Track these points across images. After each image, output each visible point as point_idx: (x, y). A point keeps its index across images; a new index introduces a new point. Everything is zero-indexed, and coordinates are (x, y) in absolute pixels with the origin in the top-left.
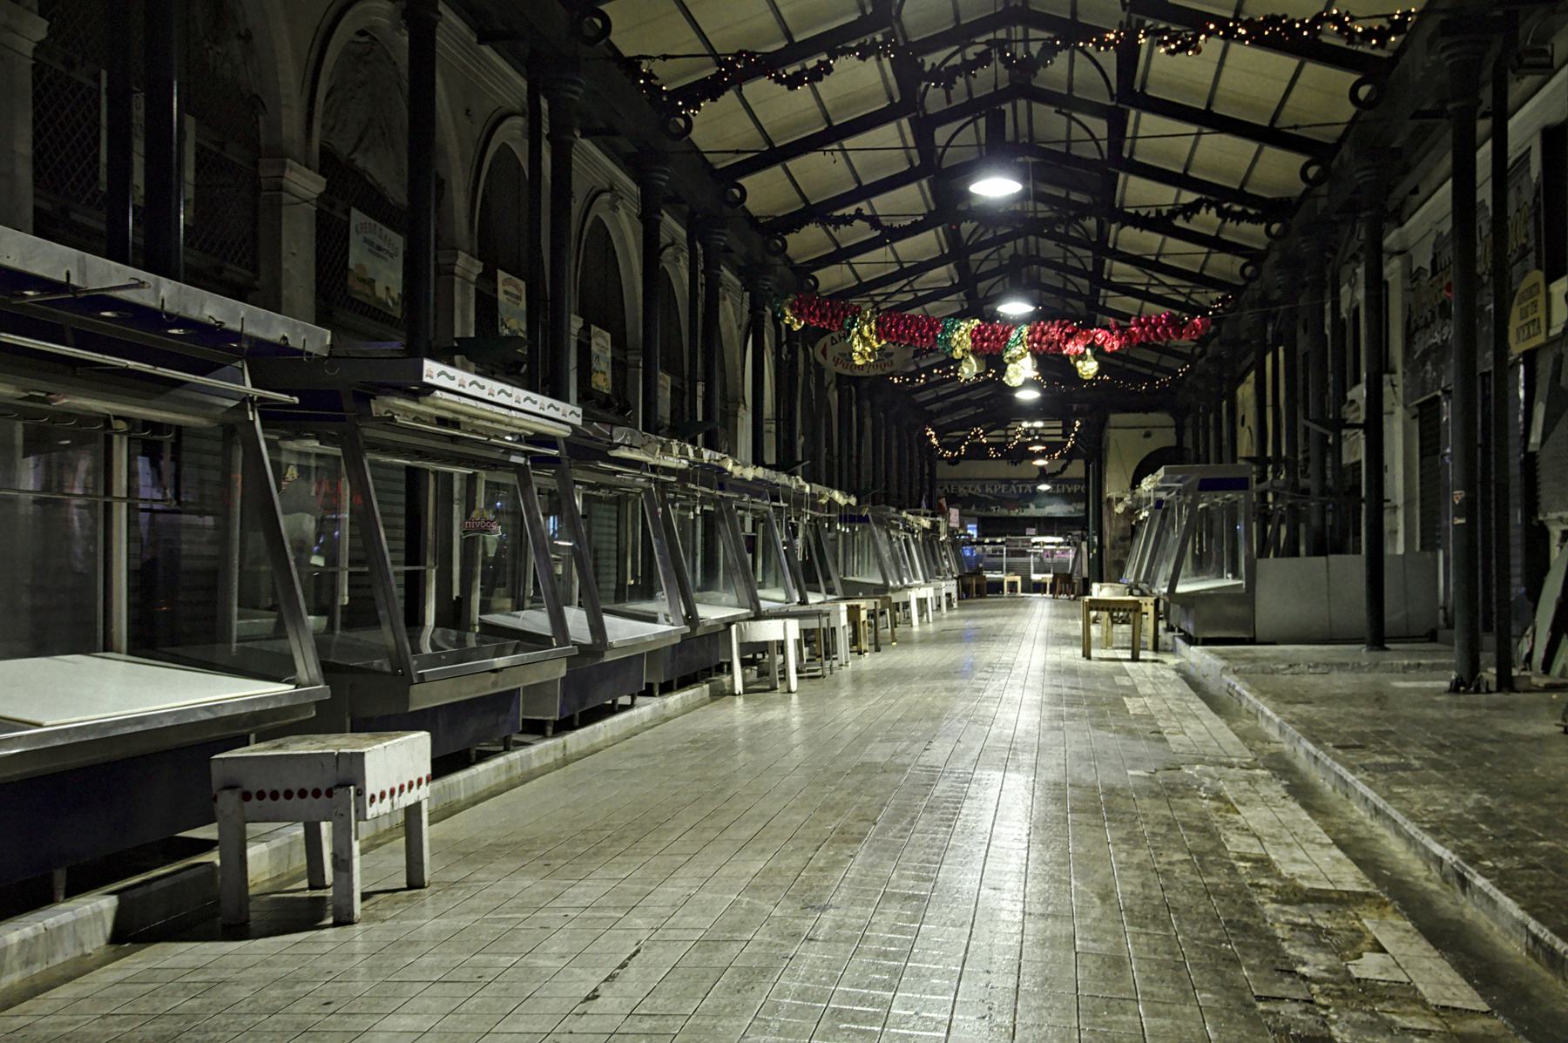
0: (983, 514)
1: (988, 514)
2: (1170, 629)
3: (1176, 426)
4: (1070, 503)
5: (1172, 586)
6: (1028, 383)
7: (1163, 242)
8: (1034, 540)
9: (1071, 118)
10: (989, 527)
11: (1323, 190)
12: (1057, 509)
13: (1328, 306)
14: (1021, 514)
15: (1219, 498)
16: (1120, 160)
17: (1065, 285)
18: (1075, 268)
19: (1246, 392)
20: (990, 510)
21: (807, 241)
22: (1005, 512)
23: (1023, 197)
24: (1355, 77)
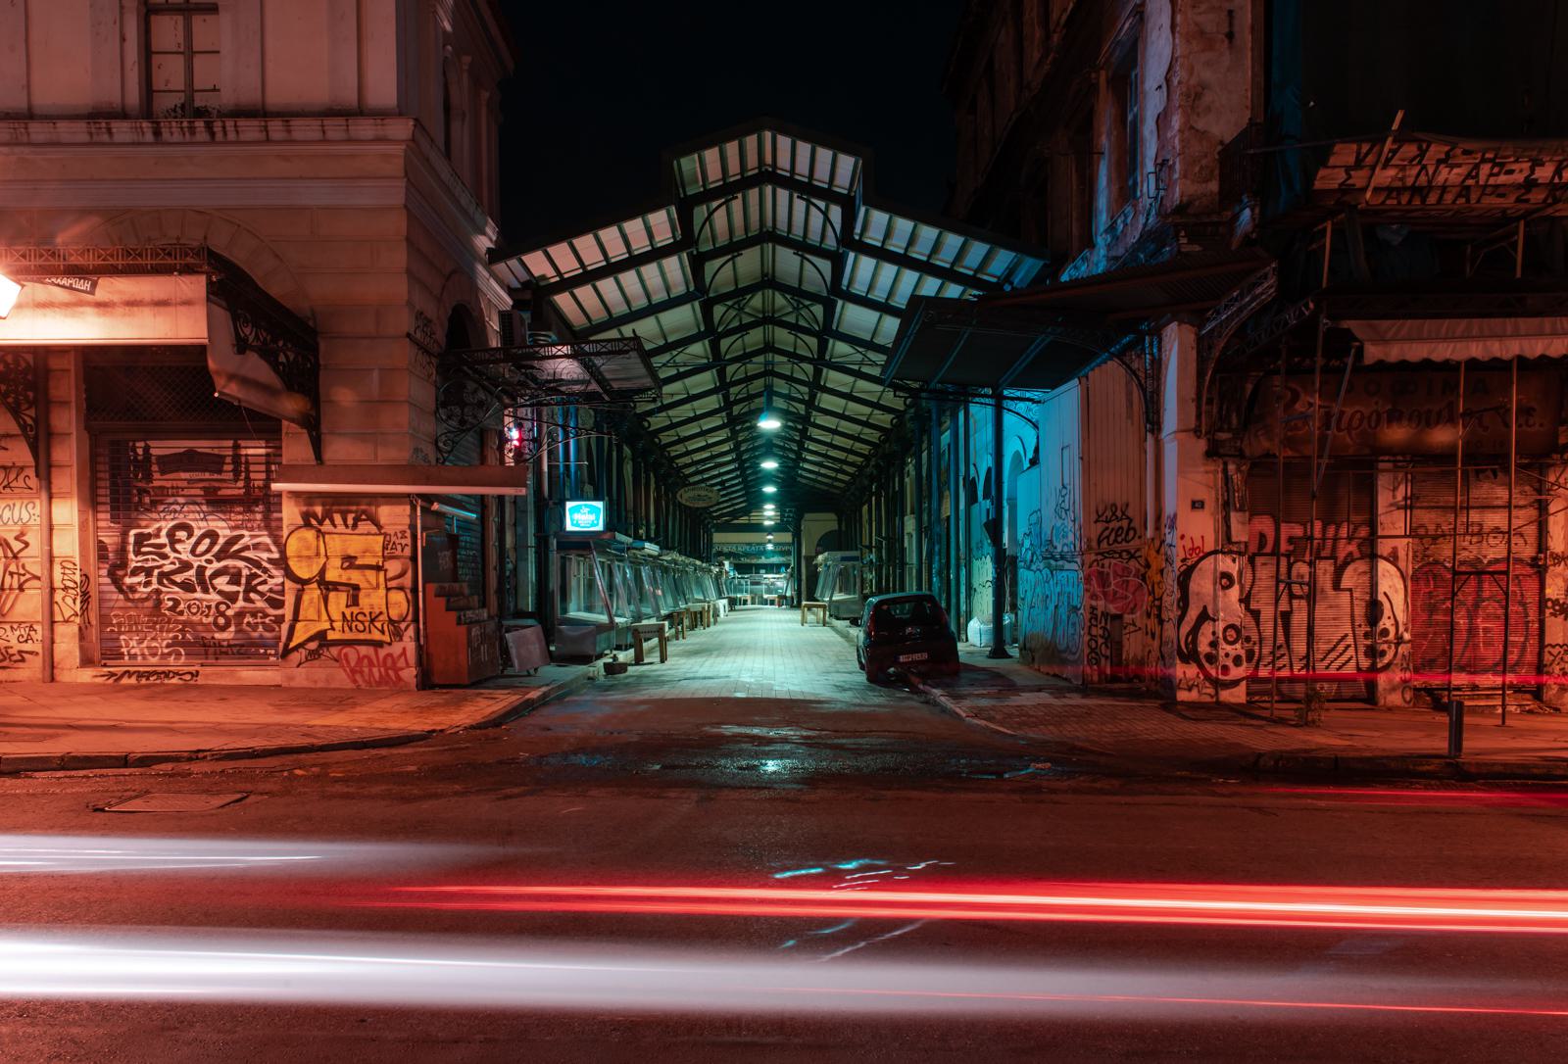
5: (831, 597)
6: (770, 519)
9: (796, 336)
10: (741, 568)
11: (912, 410)
12: (775, 560)
15: (850, 563)
16: (838, 291)
21: (687, 471)
22: (748, 561)
23: (778, 470)
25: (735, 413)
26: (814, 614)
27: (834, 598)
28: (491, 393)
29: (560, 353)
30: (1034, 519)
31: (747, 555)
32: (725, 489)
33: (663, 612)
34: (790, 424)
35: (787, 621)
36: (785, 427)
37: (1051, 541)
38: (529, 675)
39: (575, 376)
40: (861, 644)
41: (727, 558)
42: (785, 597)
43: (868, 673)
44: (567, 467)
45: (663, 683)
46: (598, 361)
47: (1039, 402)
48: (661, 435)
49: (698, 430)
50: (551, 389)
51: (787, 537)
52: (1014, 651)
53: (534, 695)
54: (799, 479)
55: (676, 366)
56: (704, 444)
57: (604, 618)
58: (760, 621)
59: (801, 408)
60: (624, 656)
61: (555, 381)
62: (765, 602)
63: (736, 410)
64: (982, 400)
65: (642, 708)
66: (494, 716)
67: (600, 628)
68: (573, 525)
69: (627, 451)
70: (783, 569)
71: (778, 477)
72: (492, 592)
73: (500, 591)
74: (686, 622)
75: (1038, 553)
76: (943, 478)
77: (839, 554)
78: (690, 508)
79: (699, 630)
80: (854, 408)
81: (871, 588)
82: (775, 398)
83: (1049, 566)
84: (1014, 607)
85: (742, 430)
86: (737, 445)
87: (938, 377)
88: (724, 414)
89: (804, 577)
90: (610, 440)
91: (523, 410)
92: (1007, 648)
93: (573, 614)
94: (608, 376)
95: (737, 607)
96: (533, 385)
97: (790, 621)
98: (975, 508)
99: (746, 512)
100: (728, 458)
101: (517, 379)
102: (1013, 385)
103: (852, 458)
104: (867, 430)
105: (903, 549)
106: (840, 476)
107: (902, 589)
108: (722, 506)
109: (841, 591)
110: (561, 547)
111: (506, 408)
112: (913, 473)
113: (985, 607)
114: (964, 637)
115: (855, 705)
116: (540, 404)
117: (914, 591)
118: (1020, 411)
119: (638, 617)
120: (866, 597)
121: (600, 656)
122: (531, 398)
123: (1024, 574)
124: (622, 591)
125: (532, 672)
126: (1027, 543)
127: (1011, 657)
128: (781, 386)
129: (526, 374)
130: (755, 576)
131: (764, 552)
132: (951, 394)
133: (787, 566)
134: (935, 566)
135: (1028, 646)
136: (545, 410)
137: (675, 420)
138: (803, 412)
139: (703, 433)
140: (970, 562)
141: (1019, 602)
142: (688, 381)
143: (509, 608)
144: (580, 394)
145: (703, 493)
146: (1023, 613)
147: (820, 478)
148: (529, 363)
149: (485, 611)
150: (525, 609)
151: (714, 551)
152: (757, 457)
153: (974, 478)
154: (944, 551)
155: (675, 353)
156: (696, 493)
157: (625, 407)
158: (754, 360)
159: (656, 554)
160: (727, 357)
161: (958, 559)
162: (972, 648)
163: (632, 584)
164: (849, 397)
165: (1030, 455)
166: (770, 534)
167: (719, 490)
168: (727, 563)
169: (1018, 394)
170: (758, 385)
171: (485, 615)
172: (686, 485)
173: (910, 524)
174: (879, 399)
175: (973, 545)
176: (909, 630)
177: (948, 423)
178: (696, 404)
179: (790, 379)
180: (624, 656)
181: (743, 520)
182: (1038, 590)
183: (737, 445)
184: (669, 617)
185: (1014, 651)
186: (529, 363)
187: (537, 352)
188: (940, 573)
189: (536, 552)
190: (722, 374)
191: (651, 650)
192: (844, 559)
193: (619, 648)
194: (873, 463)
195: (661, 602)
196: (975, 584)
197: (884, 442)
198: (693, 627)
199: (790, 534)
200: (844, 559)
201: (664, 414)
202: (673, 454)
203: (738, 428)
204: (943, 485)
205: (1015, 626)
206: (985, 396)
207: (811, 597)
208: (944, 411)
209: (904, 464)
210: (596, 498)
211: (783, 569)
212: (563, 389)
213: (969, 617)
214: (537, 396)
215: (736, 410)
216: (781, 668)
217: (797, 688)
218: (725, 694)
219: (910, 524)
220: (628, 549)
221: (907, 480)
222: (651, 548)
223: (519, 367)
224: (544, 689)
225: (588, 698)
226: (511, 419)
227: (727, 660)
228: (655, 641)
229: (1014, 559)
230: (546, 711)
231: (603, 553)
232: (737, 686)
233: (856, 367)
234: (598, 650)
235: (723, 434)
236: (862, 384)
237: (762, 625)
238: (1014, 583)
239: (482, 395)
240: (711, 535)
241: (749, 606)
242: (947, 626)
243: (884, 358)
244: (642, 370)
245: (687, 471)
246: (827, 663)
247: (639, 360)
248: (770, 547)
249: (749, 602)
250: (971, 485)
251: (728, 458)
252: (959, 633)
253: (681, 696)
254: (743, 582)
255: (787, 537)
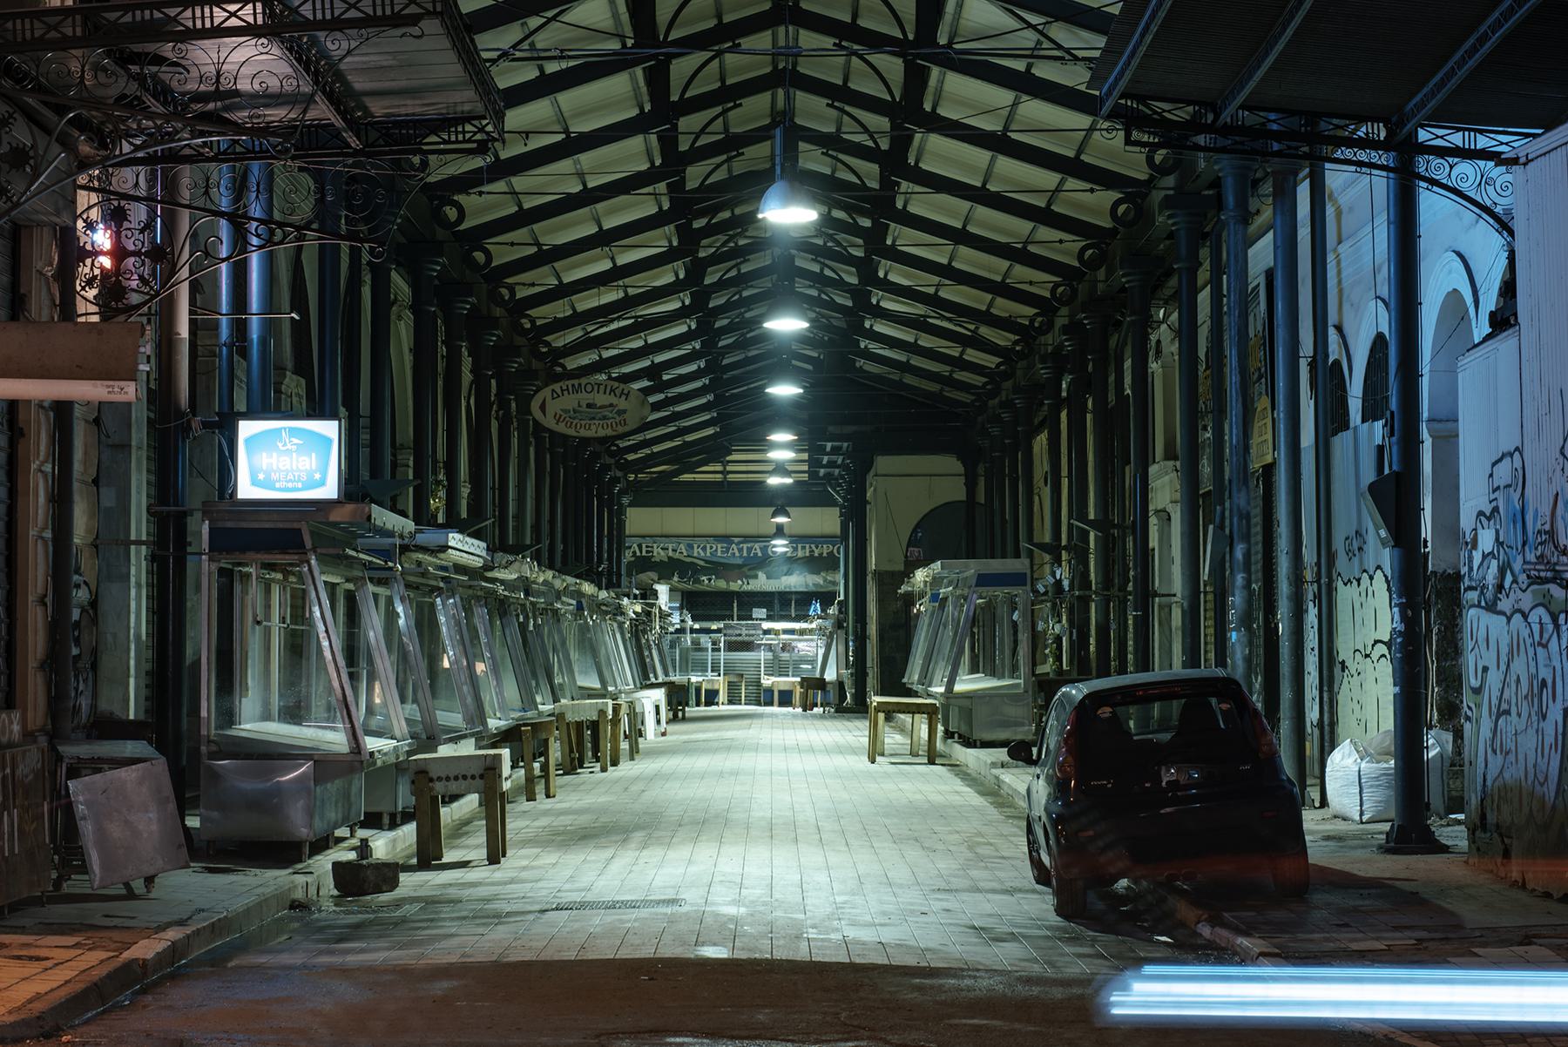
0: (689, 587)
1: (698, 587)
2: (949, 735)
3: (966, 475)
4: (817, 573)
6: (780, 469)
7: (992, 161)
8: (766, 625)
10: (698, 604)
11: (1170, 181)
12: (796, 581)
13: (1112, 378)
14: (745, 588)
15: (1000, 592)
17: (822, 270)
18: (859, 145)
19: (1041, 441)
20: (697, 581)
21: (560, 340)
22: (721, 584)
24: (1118, 195)
25: (691, 185)
26: (902, 730)
27: (959, 687)
28: (47, 131)
29: (233, 22)
30: (1504, 472)
31: (717, 568)
32: (661, 386)
33: (494, 724)
34: (839, 214)
35: (828, 751)
36: (827, 221)
37: (1552, 534)
38: (131, 895)
39: (274, 84)
40: (1039, 811)
41: (664, 577)
42: (821, 684)
43: (1058, 893)
44: (240, 328)
45: (499, 917)
46: (335, 45)
47: (1514, 161)
48: (492, 243)
49: (593, 230)
50: (205, 117)
51: (827, 520)
52: (1453, 833)
53: (146, 949)
54: (860, 363)
55: (538, 58)
56: (606, 265)
57: (334, 739)
58: (756, 748)
59: (870, 172)
60: (384, 845)
61: (218, 95)
62: (765, 697)
63: (695, 175)
64: (1363, 156)
65: (442, 986)
66: (39, 1006)
67: (325, 765)
68: (322, 483)
69: (400, 284)
70: (816, 608)
71: (807, 359)
72: (32, 664)
73: (54, 662)
74: (556, 751)
75: (1517, 565)
76: (1257, 360)
77: (972, 568)
78: (565, 437)
79: (590, 775)
80: (1013, 173)
81: (1059, 658)
82: (802, 146)
83: (1546, 602)
84: (1451, 714)
85: (709, 231)
86: (697, 270)
87: (1241, 98)
88: (662, 187)
89: (872, 629)
90: (355, 254)
91: (128, 173)
92: (1434, 823)
93: (253, 724)
94: (359, 83)
95: (691, 711)
96: (159, 109)
97: (840, 750)
98: (1341, 444)
99: (716, 450)
100: (673, 305)
101: (113, 92)
102: (1443, 117)
103: (1004, 307)
104: (1045, 233)
105: (1145, 554)
106: (972, 355)
107: (1144, 664)
108: (650, 434)
109: (974, 669)
110: (224, 542)
111: (84, 165)
112: (1172, 348)
113: (1370, 712)
114: (1314, 794)
115: (1029, 981)
116: (175, 157)
117: (1178, 669)
118: (1464, 186)
119: (428, 737)
120: (1046, 688)
121: (323, 844)
122: (152, 139)
123: (1476, 621)
124: (385, 664)
125: (138, 886)
126: (1486, 540)
127: (1444, 849)
128: (813, 111)
129: (140, 79)
130: (741, 629)
131: (763, 562)
132: (1278, 136)
133: (827, 598)
134: (1236, 600)
135: (1491, 818)
136: (187, 176)
137: (528, 204)
138: (875, 185)
139: (604, 238)
140: (1331, 589)
141: (1467, 699)
142: (568, 99)
143: (76, 710)
144: (287, 130)
145: (601, 399)
146: (1479, 731)
147: (917, 361)
148: (151, 47)
149: (16, 715)
150: (118, 713)
151: (628, 556)
152: (748, 303)
153: (1337, 363)
154: (1257, 558)
155: (534, 22)
156: (585, 398)
157: (396, 164)
158: (746, 43)
159: (478, 563)
160: (673, 36)
161: (1297, 581)
162: (1341, 826)
163: (412, 647)
164: (999, 143)
165: (1490, 301)
166: (780, 511)
167: (646, 391)
168: (663, 590)
169: (1457, 139)
170: (755, 109)
171: (16, 728)
172: (557, 378)
173: (1165, 487)
174: (1080, 151)
175: (1338, 544)
176: (1170, 774)
177: (1267, 214)
178: (586, 159)
179: (839, 94)
180: (384, 845)
181: (709, 473)
182: (1519, 666)
183: (697, 270)
184: (509, 736)
185: (1453, 833)
186: (151, 47)
187: (175, 20)
188: (1246, 621)
189: (152, 558)
190: (658, 80)
191: (461, 828)
192: (984, 580)
193: (373, 821)
194: (1060, 321)
195: (489, 696)
196: (1344, 649)
197: (1093, 264)
198: (572, 766)
199: (836, 511)
200: (984, 580)
201: (500, 186)
202: (522, 293)
203: (699, 224)
204: (1257, 377)
205: (1455, 763)
206: (1367, 143)
207: (893, 683)
208: (1256, 184)
209: (1146, 324)
210: (316, 411)
211: (816, 608)
212: (241, 116)
213: (1329, 742)
214: (171, 136)
215: (695, 175)
216: (822, 878)
217: (866, 935)
218: (668, 951)
219: (1165, 487)
220: (405, 549)
221: (1154, 366)
222: (465, 548)
223: (124, 59)
224: (173, 934)
225: (296, 959)
226: (94, 198)
227: (672, 854)
228: (471, 802)
229: (1452, 581)
230: (177, 995)
231: (335, 560)
232: (702, 928)
233: (1019, 65)
234: (319, 826)
235: (659, 241)
236: (1036, 110)
237: (762, 762)
238: (1452, 647)
239: (21, 134)
240: (621, 512)
241: (724, 709)
242: (1273, 759)
243: (1101, 41)
244: (448, 67)
245: (560, 340)
246: (945, 865)
247: (447, 44)
248: (780, 546)
249: (722, 697)
250: (1330, 380)
251: (673, 305)
252: (1303, 786)
253: (547, 956)
254: (705, 641)
255: (827, 520)
